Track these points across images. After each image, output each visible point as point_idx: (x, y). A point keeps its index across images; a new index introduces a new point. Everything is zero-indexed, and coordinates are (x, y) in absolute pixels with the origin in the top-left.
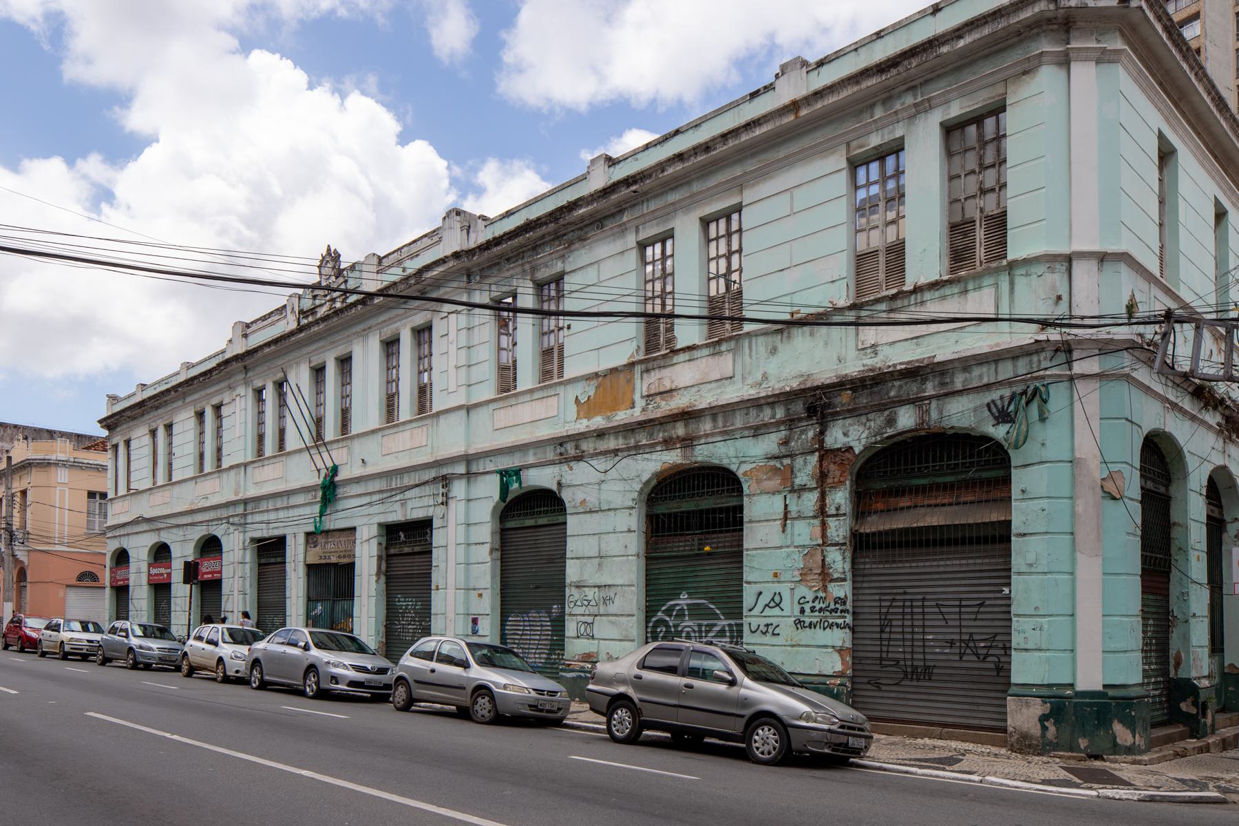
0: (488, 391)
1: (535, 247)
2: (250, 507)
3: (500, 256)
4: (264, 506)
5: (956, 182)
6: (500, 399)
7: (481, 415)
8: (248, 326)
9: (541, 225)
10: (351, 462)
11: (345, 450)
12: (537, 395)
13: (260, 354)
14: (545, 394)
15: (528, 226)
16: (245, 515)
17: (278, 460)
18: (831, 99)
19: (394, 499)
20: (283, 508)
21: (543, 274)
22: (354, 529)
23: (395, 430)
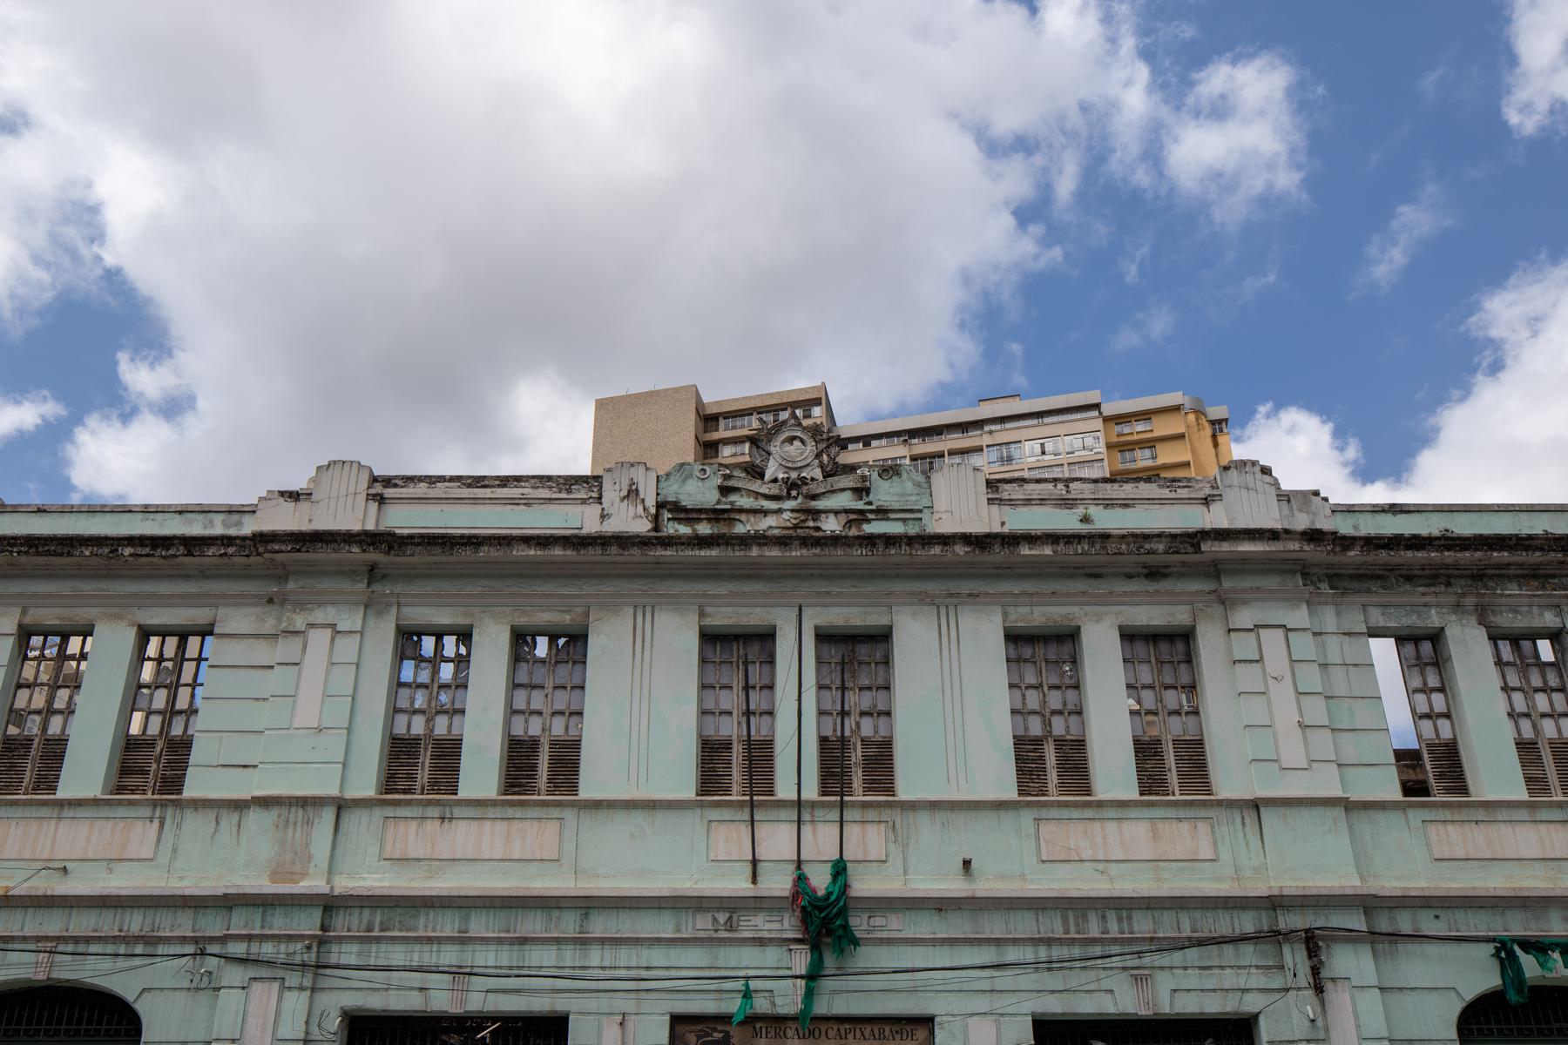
0: (365, 783)
1: (1501, 574)
2: (343, 923)
3: (1392, 568)
4: (426, 924)
5: (766, 681)
6: (108, 803)
7: (360, 825)
8: (388, 482)
9: (1527, 548)
10: (892, 862)
11: (552, 827)
12: (491, 812)
13: (484, 553)
14: (510, 812)
15: (1450, 542)
16: (322, 941)
17: (105, 812)
18: (1247, 547)
19: (1116, 962)
20: (603, 941)
21: (1506, 620)
22: (927, 1021)
23: (1088, 813)
